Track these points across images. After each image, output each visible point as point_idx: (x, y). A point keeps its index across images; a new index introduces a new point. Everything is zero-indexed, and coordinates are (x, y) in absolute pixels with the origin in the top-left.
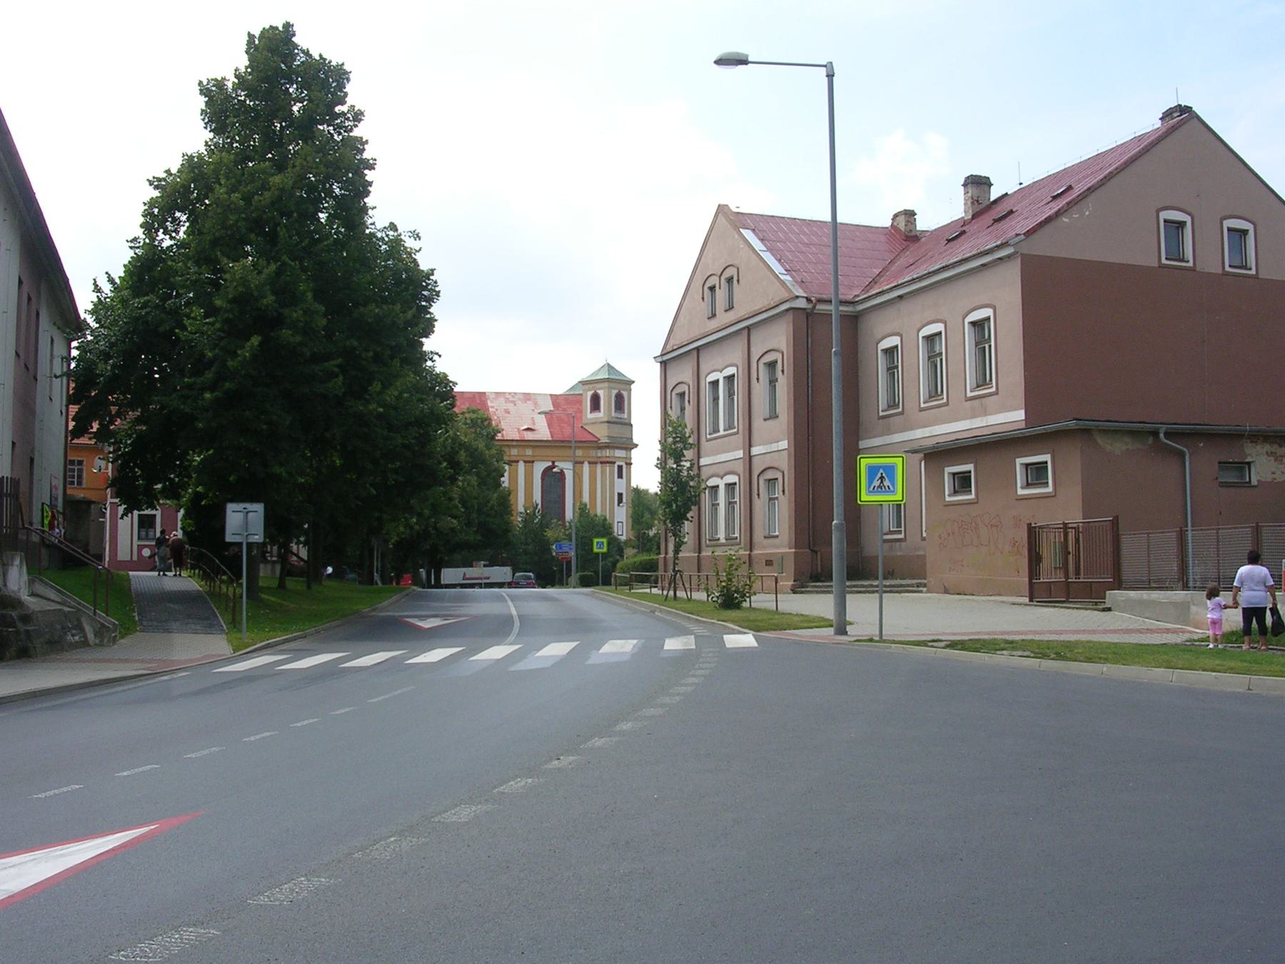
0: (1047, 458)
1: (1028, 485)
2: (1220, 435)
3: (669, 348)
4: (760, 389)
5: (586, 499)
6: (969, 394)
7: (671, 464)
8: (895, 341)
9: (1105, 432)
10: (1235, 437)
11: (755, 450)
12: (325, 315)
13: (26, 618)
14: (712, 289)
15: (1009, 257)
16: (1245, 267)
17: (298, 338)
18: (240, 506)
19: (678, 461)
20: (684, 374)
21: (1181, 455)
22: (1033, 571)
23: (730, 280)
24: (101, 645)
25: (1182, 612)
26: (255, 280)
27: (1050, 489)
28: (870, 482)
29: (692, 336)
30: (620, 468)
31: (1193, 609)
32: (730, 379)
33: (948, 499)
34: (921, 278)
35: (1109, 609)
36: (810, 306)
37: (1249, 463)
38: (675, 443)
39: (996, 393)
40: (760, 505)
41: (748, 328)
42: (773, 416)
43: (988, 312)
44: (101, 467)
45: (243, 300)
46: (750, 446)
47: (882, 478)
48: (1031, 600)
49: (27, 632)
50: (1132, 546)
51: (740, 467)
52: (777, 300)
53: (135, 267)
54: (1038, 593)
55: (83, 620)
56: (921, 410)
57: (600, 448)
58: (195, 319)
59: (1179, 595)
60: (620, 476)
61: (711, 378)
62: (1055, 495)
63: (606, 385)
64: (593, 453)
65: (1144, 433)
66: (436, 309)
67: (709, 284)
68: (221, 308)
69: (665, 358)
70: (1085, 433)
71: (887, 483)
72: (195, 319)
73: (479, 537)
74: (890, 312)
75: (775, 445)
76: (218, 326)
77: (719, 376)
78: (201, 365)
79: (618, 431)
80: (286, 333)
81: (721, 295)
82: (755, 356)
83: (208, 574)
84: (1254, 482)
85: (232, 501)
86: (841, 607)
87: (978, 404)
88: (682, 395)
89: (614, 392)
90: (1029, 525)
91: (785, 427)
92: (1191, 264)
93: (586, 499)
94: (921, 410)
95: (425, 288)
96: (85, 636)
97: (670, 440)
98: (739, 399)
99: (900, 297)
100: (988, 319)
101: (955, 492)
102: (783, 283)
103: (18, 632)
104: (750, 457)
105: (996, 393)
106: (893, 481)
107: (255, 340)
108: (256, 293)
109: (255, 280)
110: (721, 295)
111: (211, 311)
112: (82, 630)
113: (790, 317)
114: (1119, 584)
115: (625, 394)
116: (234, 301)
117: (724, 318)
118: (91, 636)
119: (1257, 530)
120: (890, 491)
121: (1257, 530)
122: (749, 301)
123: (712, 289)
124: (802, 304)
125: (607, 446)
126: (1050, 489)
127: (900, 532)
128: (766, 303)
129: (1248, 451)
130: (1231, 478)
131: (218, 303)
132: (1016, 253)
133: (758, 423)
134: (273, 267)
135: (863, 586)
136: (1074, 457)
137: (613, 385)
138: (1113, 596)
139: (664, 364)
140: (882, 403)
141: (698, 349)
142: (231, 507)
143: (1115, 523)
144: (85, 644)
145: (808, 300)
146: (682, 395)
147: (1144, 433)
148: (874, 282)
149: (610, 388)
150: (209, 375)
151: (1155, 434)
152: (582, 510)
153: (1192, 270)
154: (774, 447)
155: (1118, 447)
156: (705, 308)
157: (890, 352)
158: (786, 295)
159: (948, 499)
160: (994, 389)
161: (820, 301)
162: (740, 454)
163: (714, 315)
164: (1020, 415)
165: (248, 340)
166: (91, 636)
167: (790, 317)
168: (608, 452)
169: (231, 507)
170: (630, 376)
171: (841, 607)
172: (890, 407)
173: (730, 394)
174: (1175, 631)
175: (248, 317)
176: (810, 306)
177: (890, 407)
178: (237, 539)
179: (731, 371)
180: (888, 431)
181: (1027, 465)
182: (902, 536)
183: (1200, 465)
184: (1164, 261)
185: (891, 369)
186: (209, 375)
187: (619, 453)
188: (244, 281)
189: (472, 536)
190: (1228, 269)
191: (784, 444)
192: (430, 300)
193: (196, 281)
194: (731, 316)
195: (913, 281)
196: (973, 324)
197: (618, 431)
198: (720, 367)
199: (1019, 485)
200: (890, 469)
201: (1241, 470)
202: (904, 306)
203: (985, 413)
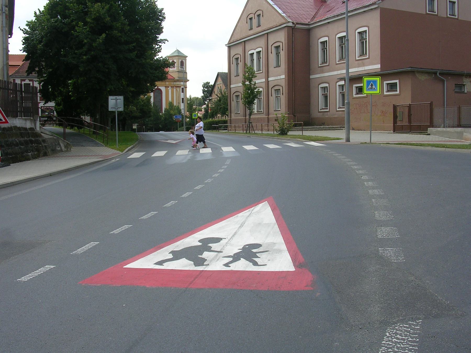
0: (397, 81)
1: (388, 91)
2: (446, 74)
3: (231, 41)
4: (272, 57)
5: (170, 99)
6: (357, 59)
7: (247, 83)
8: (326, 39)
9: (419, 72)
10: (461, 75)
11: (270, 79)
12: (129, 25)
13: (44, 141)
14: (251, 19)
15: (375, 8)
16: (454, 15)
17: (120, 34)
18: (114, 97)
19: (250, 82)
20: (239, 50)
21: (443, 81)
22: (395, 122)
23: (259, 16)
24: (67, 151)
25: (460, 136)
26: (102, 12)
27: (398, 92)
28: (368, 86)
29: (242, 37)
30: (183, 89)
31: (465, 134)
32: (259, 53)
33: (354, 96)
34: (338, 16)
35: (429, 134)
36: (294, 25)
37: (464, 85)
38: (249, 75)
39: (369, 58)
40: (272, 99)
41: (267, 34)
42: (278, 66)
43: (366, 29)
44: (31, 85)
45: (98, 19)
46: (268, 77)
47: (372, 85)
48: (394, 132)
49: (45, 146)
50: (437, 112)
51: (264, 85)
52: (280, 23)
53: (49, 6)
54: (397, 129)
55: (60, 142)
56: (337, 64)
57: (175, 81)
58: (80, 27)
59: (459, 129)
60: (183, 92)
61: (251, 52)
62: (403, 94)
63: (177, 58)
64: (172, 83)
65: (432, 73)
66: (164, 24)
67: (250, 17)
68: (89, 22)
69: (230, 45)
70: (412, 72)
71: (374, 87)
72: (80, 27)
73: (140, 114)
74: (324, 28)
75: (279, 77)
76: (88, 29)
77: (255, 52)
78: (80, 45)
79: (181, 75)
80: (115, 32)
81: (255, 21)
82: (270, 43)
83: (79, 128)
84: (466, 92)
85: (110, 95)
86: (348, 134)
87: (361, 62)
88: (237, 59)
89: (180, 60)
90: (394, 105)
91: (283, 70)
92: (436, 13)
93: (170, 99)
94: (337, 64)
95: (160, 16)
96: (61, 148)
97: (247, 74)
98: (263, 60)
99: (329, 23)
100: (365, 31)
101: (357, 94)
102: (283, 17)
103: (42, 146)
104: (268, 81)
105: (369, 58)
106: (376, 86)
107: (104, 35)
108: (102, 17)
109: (102, 12)
110: (255, 21)
111: (86, 23)
112: (60, 145)
113: (286, 29)
114: (432, 125)
115: (184, 61)
116: (93, 19)
117: (256, 30)
118: (63, 148)
119: (459, 108)
120: (375, 90)
121: (459, 108)
122: (266, 24)
123: (251, 19)
124: (290, 24)
125: (178, 81)
126: (398, 92)
127: (327, 109)
128: (275, 24)
129: (464, 80)
130: (457, 90)
131: (88, 20)
132: (378, 7)
133: (271, 69)
134: (108, 6)
135: (333, 128)
136: (409, 82)
137: (180, 58)
138: (430, 130)
139: (229, 47)
140: (320, 62)
141: (245, 41)
142: (110, 98)
143: (431, 104)
144: (61, 151)
145: (293, 23)
146: (237, 59)
147: (432, 73)
148: (314, 17)
149: (179, 59)
150: (85, 49)
151: (435, 73)
152: (171, 104)
153: (437, 15)
154: (279, 77)
155: (423, 78)
156: (248, 26)
157: (324, 43)
158: (284, 21)
159: (354, 96)
160: (368, 57)
161: (297, 24)
162: (264, 80)
163: (251, 29)
164: (379, 66)
165: (101, 35)
166: (63, 148)
167: (286, 29)
168: (178, 83)
169: (110, 98)
170: (186, 54)
171: (348, 134)
172: (322, 63)
173: (259, 58)
174: (460, 141)
175: (100, 27)
176: (294, 25)
177: (322, 63)
178: (114, 110)
179: (259, 49)
180: (323, 72)
181: (388, 84)
182: (328, 110)
183: (449, 84)
184: (427, 12)
185: (324, 50)
186: (85, 49)
187: (182, 83)
188: (98, 11)
189: (138, 114)
190: (448, 16)
191: (283, 77)
192: (162, 20)
193: (77, 12)
194: (260, 29)
195: (334, 17)
196: (359, 33)
197: (181, 75)
198: (254, 49)
199: (354, 94)
200: (375, 82)
201: (461, 87)
202: (330, 26)
203: (364, 65)
